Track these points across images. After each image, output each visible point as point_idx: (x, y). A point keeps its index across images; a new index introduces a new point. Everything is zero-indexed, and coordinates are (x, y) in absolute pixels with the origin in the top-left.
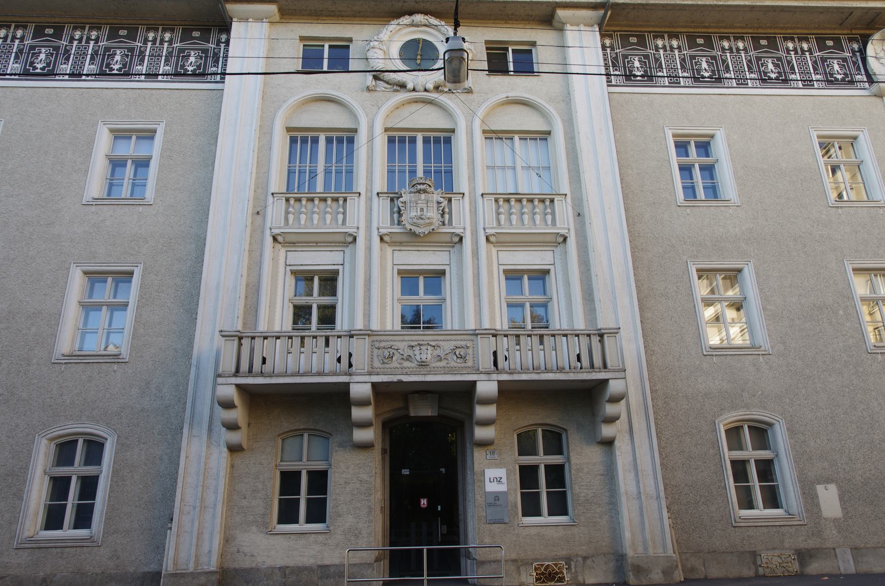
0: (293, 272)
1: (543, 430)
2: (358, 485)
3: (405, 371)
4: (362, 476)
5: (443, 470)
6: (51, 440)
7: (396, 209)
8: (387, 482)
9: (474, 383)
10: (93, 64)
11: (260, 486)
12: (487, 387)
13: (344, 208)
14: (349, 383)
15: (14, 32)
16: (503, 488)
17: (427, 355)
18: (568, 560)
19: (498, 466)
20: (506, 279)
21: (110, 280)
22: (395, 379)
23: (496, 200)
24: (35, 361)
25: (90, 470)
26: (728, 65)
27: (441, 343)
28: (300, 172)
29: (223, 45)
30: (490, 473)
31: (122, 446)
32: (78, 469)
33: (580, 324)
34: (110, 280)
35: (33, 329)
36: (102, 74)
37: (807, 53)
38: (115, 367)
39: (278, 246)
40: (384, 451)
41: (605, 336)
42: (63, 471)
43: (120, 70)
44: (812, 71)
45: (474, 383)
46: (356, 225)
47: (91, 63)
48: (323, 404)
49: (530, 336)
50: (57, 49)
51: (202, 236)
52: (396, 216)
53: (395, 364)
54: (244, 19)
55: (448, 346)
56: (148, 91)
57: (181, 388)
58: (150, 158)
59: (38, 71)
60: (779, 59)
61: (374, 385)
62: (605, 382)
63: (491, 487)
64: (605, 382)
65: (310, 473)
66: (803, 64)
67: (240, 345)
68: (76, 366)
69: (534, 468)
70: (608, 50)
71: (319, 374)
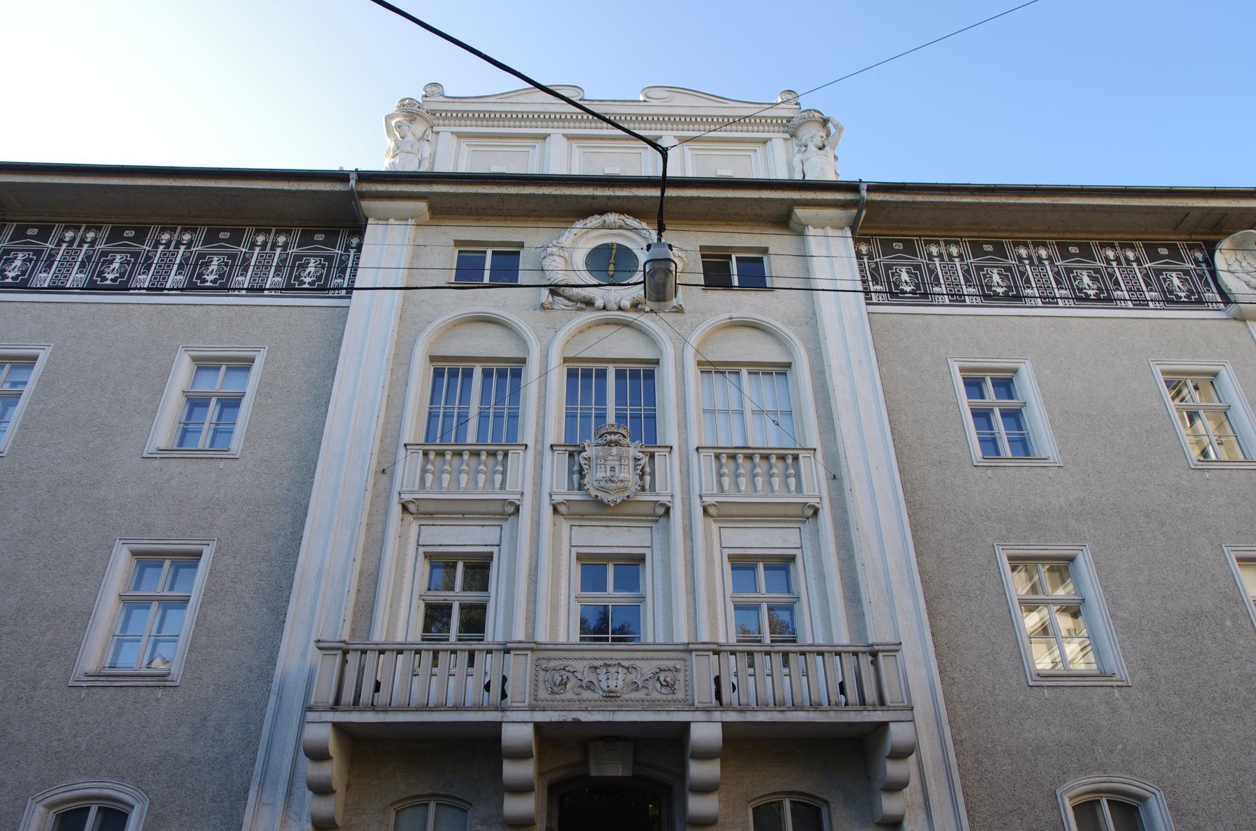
0: (428, 556)
3: (584, 705)
6: (49, 807)
7: (576, 468)
9: (686, 726)
12: (706, 732)
13: (504, 466)
14: (500, 723)
17: (617, 681)
20: (733, 568)
21: (167, 563)
22: (569, 717)
23: (717, 457)
24: (44, 683)
27: (638, 663)
28: (445, 416)
29: (352, 251)
33: (842, 637)
34: (167, 563)
35: (49, 635)
37: (1135, 265)
39: (409, 518)
45: (686, 726)
46: (519, 490)
52: (576, 477)
53: (569, 695)
54: (384, 218)
57: (252, 727)
59: (306, 286)
61: (538, 726)
67: (345, 662)
71: (458, 708)
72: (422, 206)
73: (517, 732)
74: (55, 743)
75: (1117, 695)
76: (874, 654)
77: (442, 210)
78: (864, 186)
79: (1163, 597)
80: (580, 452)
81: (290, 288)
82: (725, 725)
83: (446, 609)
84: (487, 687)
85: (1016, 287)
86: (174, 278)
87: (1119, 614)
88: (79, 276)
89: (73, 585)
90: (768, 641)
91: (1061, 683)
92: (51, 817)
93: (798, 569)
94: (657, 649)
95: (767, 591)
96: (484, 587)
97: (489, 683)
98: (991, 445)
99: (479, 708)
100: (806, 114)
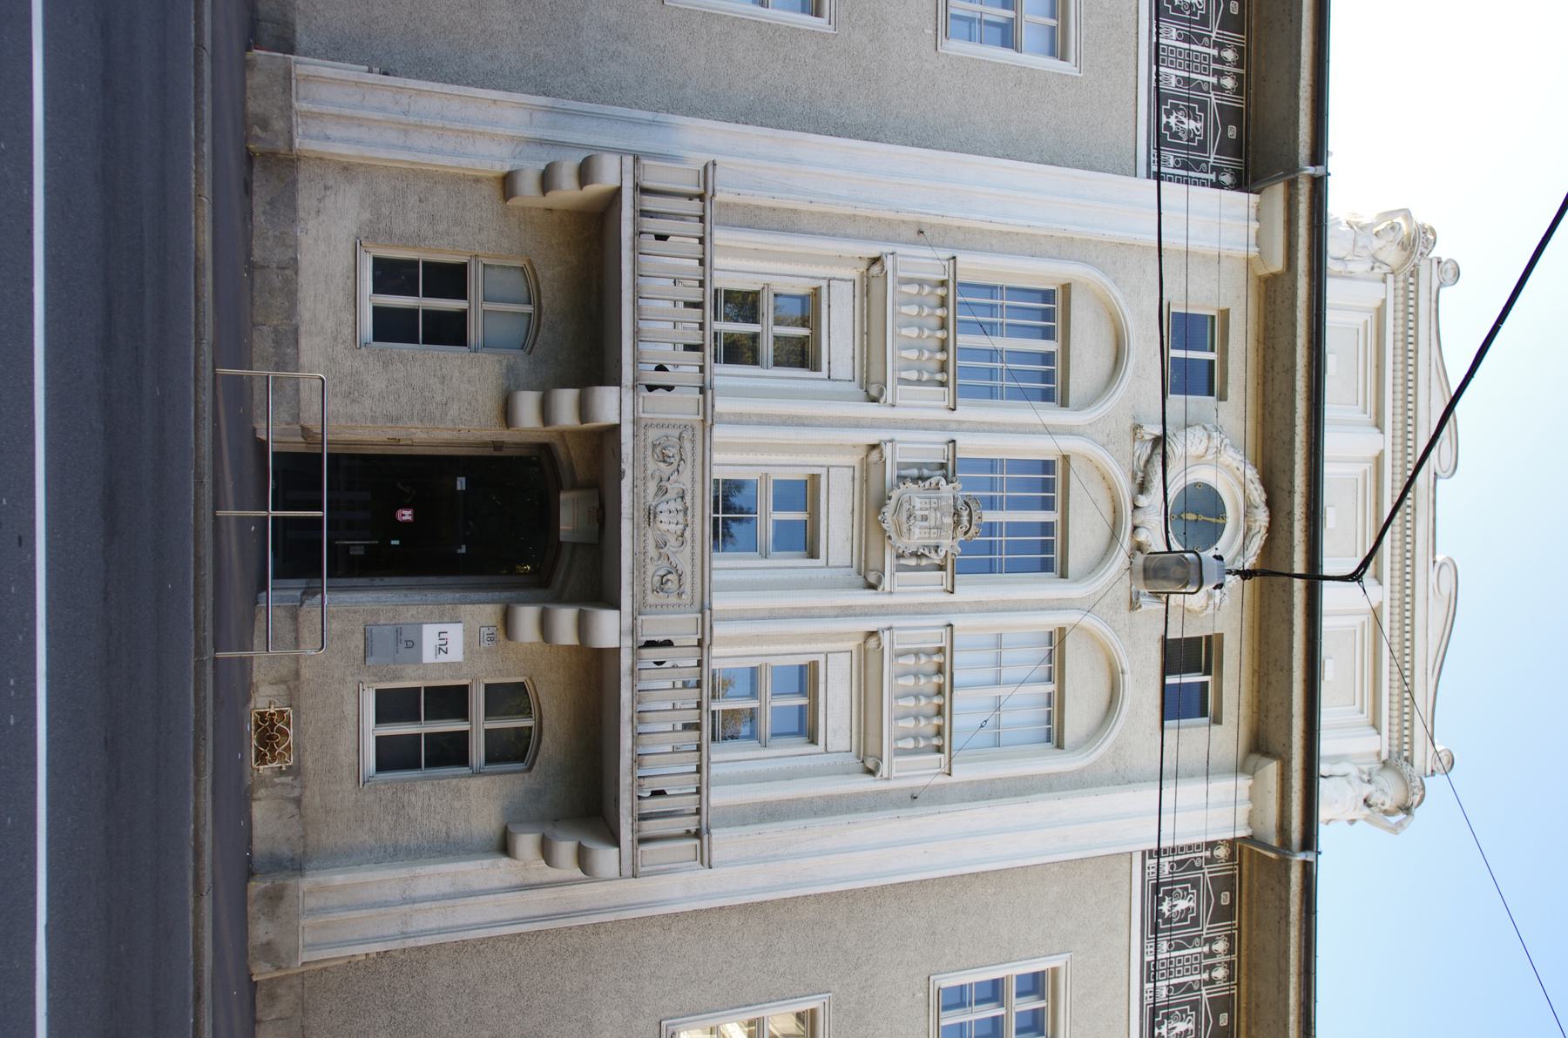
1: (530, 728)
2: (438, 399)
3: (639, 483)
4: (456, 406)
7: (926, 472)
9: (615, 605)
11: (440, 228)
14: (619, 384)
16: (429, 655)
18: (296, 771)
19: (468, 646)
20: (801, 667)
22: (626, 466)
23: (940, 650)
27: (688, 547)
29: (1212, 177)
30: (455, 633)
33: (719, 797)
39: (863, 266)
40: (498, 445)
41: (697, 842)
44: (1173, 981)
45: (615, 605)
46: (899, 402)
48: (585, 341)
49: (699, 705)
52: (915, 472)
53: (652, 465)
56: (1133, 48)
59: (1164, 119)
61: (615, 429)
63: (430, 634)
65: (462, 316)
67: (691, 197)
69: (463, 714)
71: (636, 332)
72: (1277, 264)
76: (697, 835)
78: (1310, 857)
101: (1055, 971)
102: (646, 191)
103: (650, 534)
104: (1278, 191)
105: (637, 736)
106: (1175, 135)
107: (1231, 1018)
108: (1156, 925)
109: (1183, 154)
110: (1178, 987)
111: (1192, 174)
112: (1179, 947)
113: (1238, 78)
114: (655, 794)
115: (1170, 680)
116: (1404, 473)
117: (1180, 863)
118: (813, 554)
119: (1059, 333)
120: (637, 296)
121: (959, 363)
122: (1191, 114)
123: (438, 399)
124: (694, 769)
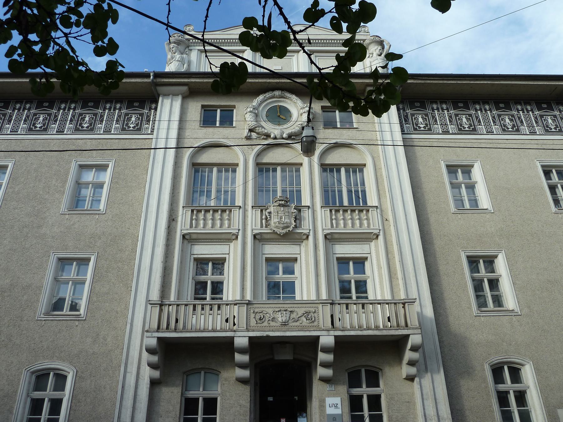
1: (366, 370)
2: (238, 409)
3: (271, 329)
4: (241, 402)
5: (296, 398)
7: (264, 217)
8: (258, 406)
9: (318, 337)
10: (117, 124)
11: (171, 408)
12: (327, 340)
13: (229, 215)
14: (233, 337)
15: (70, 105)
16: (339, 411)
19: (334, 396)
20: (338, 263)
21: (75, 263)
22: (265, 334)
24: (25, 318)
25: (57, 395)
26: (480, 120)
27: (296, 309)
28: (207, 191)
29: (153, 111)
30: (329, 401)
31: (78, 378)
32: (49, 394)
33: (388, 297)
34: (75, 263)
35: (25, 297)
36: (30, 130)
37: (531, 112)
38: (77, 323)
39: (186, 242)
40: (256, 384)
41: (406, 304)
42: (38, 395)
43: (88, 127)
44: (449, 124)
45: (318, 337)
46: (237, 228)
47: (70, 123)
48: (218, 350)
49: (355, 304)
50: (142, 115)
51: (136, 234)
52: (264, 221)
53: (265, 324)
54: (166, 95)
55: (301, 311)
56: (105, 140)
57: (119, 338)
58: (104, 183)
59: (131, 129)
60: (513, 116)
61: (250, 338)
62: (407, 337)
63: (330, 411)
64: (407, 337)
65: (205, 400)
66: (528, 120)
67: (161, 310)
68: (52, 322)
70: (401, 111)
72: (185, 88)
73: (241, 341)
74: (33, 345)
75: (514, 319)
76: (404, 304)
77: (193, 92)
79: (538, 274)
80: (266, 209)
81: (30, 129)
82: (336, 337)
83: (204, 284)
84: (227, 321)
85: (474, 126)
86: (22, 125)
87: (517, 282)
88: (24, 126)
89: (34, 274)
90: (354, 298)
91: (489, 315)
92: (34, 377)
93: (367, 264)
94: (303, 303)
95: (355, 274)
96: (221, 273)
97: (227, 318)
98: (474, 202)
99: (222, 330)
100: (372, 38)
101: (542, 166)
102: (159, 327)
103: (291, 324)
104: (161, 89)
105: (368, 328)
106: (137, 125)
107: (544, 103)
108: (473, 131)
109: (144, 122)
110: (450, 121)
111: (151, 119)
112: (436, 121)
113: (26, 103)
114: (389, 321)
115: (339, 126)
116: (217, 43)
117: (406, 121)
118: (224, 260)
119: (331, 167)
120: (214, 330)
121: (222, 205)
122: (83, 119)
123: (238, 409)
124: (355, 306)
